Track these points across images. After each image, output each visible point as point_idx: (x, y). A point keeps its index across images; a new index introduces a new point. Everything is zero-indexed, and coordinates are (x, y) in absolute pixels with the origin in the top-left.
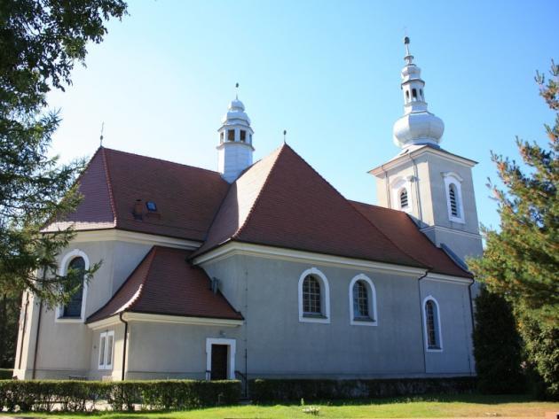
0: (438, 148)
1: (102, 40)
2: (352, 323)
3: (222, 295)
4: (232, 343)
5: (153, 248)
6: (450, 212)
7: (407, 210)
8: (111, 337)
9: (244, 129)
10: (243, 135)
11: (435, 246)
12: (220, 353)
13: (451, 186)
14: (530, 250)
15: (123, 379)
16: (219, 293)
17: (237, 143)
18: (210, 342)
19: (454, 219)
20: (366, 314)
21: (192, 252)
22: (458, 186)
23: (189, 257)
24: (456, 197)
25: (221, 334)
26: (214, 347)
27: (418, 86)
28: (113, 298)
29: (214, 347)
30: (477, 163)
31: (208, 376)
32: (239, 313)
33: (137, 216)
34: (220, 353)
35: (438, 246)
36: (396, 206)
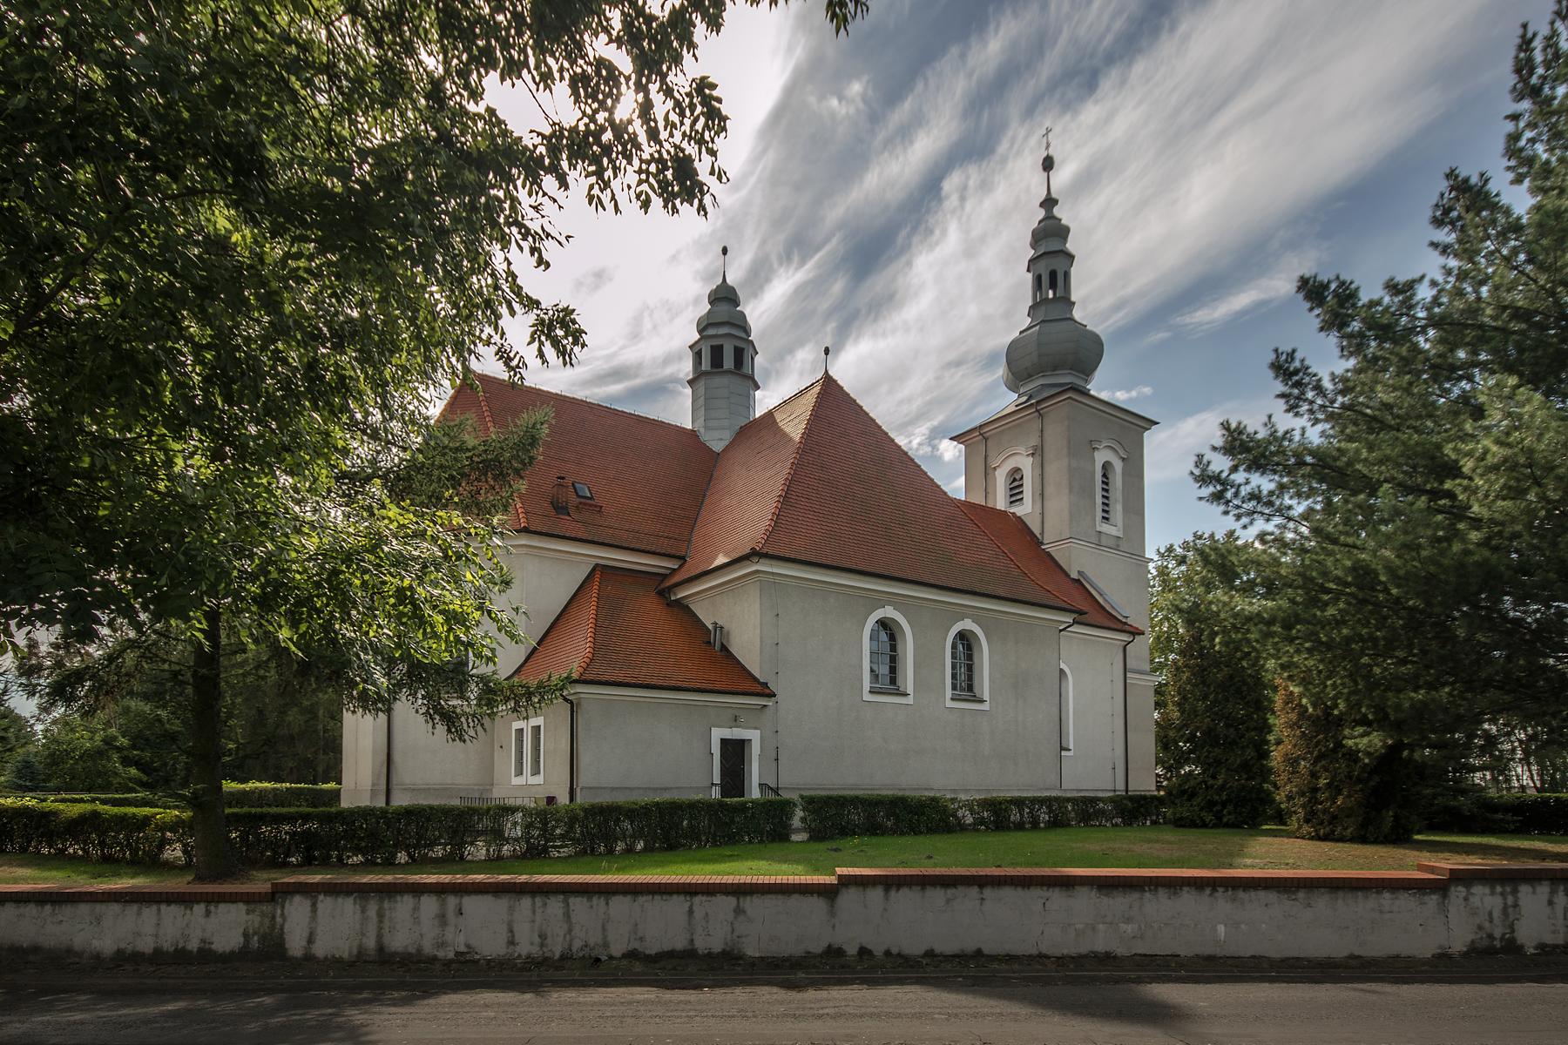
0: (1086, 394)
1: (725, 119)
2: (950, 704)
3: (727, 650)
4: (753, 735)
5: (594, 569)
6: (1099, 514)
7: (1019, 510)
8: (537, 729)
9: (741, 344)
10: (739, 354)
11: (1067, 575)
12: (734, 752)
13: (1106, 466)
14: (1233, 588)
15: (572, 799)
16: (724, 648)
17: (555, 367)
18: (718, 734)
19: (1105, 528)
20: (970, 688)
21: (665, 576)
22: (1118, 466)
23: (662, 587)
24: (1110, 488)
25: (735, 721)
26: (725, 742)
27: (1058, 264)
28: (526, 661)
29: (725, 742)
30: (1270, 417)
31: (715, 794)
32: (765, 685)
33: (560, 508)
34: (734, 752)
35: (1074, 575)
36: (1001, 503)
